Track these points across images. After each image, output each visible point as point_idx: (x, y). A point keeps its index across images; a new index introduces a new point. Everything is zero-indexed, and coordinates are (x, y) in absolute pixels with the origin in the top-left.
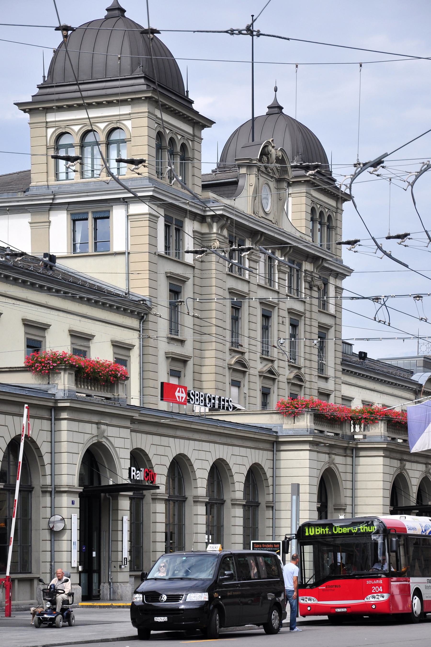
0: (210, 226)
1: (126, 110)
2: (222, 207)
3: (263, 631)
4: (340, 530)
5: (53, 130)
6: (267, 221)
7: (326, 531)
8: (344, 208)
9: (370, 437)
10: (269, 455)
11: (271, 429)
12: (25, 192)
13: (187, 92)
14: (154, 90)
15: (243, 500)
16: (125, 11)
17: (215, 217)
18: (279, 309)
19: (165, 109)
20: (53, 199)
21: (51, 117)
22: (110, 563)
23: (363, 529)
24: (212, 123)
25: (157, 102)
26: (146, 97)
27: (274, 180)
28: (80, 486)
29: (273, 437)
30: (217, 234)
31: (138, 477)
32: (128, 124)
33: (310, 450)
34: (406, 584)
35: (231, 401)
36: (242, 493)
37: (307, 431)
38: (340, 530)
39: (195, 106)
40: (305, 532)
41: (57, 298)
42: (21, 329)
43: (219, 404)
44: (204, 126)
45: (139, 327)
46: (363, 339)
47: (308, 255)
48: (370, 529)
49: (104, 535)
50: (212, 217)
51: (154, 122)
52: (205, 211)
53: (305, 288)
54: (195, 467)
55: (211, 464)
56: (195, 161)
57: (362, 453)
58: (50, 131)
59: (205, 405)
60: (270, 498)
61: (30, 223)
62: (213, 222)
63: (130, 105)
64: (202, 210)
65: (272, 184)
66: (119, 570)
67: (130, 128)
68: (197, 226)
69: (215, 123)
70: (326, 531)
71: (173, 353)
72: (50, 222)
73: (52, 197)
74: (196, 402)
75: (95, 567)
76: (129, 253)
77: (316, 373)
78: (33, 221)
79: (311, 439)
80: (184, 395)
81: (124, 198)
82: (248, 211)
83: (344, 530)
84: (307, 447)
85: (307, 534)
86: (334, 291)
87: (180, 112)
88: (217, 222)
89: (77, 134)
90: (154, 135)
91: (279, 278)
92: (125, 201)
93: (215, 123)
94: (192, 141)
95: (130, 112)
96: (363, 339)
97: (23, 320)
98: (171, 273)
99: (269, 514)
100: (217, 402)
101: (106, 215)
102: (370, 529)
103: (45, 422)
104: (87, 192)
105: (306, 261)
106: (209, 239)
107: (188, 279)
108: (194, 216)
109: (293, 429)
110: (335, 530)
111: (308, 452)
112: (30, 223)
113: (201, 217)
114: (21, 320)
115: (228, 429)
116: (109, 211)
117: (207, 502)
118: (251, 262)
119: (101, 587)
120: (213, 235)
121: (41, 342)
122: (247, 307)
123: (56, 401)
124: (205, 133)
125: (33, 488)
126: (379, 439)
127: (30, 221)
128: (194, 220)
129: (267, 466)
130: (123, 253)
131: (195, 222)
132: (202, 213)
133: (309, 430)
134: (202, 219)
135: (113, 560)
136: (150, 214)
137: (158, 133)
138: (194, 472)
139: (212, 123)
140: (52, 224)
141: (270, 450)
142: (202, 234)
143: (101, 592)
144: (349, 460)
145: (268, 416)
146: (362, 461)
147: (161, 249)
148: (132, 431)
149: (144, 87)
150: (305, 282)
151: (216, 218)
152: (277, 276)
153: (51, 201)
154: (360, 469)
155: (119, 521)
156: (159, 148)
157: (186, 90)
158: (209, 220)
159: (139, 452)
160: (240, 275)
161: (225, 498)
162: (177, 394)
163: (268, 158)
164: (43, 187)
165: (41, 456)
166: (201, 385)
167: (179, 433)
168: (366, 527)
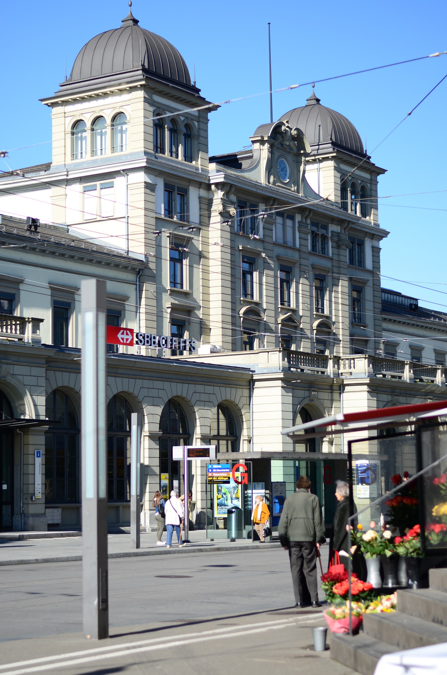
1: (126, 97)
3: (318, 558)
8: (209, 117)
9: (355, 374)
12: (45, 171)
13: (366, 151)
16: (320, 100)
17: (219, 185)
22: (22, 496)
26: (332, 157)
27: (292, 155)
37: (280, 369)
39: (372, 160)
47: (333, 218)
50: (217, 184)
53: (332, 247)
58: (68, 119)
66: (30, 502)
69: (387, 171)
72: (66, 195)
73: (66, 173)
76: (128, 217)
86: (198, 202)
89: (88, 120)
93: (387, 171)
104: (93, 167)
105: (332, 224)
107: (368, 281)
109: (267, 368)
113: (206, 185)
119: (14, 518)
122: (262, 263)
124: (380, 178)
130: (124, 217)
133: (281, 368)
135: (25, 492)
137: (362, 187)
143: (14, 523)
150: (332, 242)
157: (364, 149)
160: (323, 254)
164: (61, 166)
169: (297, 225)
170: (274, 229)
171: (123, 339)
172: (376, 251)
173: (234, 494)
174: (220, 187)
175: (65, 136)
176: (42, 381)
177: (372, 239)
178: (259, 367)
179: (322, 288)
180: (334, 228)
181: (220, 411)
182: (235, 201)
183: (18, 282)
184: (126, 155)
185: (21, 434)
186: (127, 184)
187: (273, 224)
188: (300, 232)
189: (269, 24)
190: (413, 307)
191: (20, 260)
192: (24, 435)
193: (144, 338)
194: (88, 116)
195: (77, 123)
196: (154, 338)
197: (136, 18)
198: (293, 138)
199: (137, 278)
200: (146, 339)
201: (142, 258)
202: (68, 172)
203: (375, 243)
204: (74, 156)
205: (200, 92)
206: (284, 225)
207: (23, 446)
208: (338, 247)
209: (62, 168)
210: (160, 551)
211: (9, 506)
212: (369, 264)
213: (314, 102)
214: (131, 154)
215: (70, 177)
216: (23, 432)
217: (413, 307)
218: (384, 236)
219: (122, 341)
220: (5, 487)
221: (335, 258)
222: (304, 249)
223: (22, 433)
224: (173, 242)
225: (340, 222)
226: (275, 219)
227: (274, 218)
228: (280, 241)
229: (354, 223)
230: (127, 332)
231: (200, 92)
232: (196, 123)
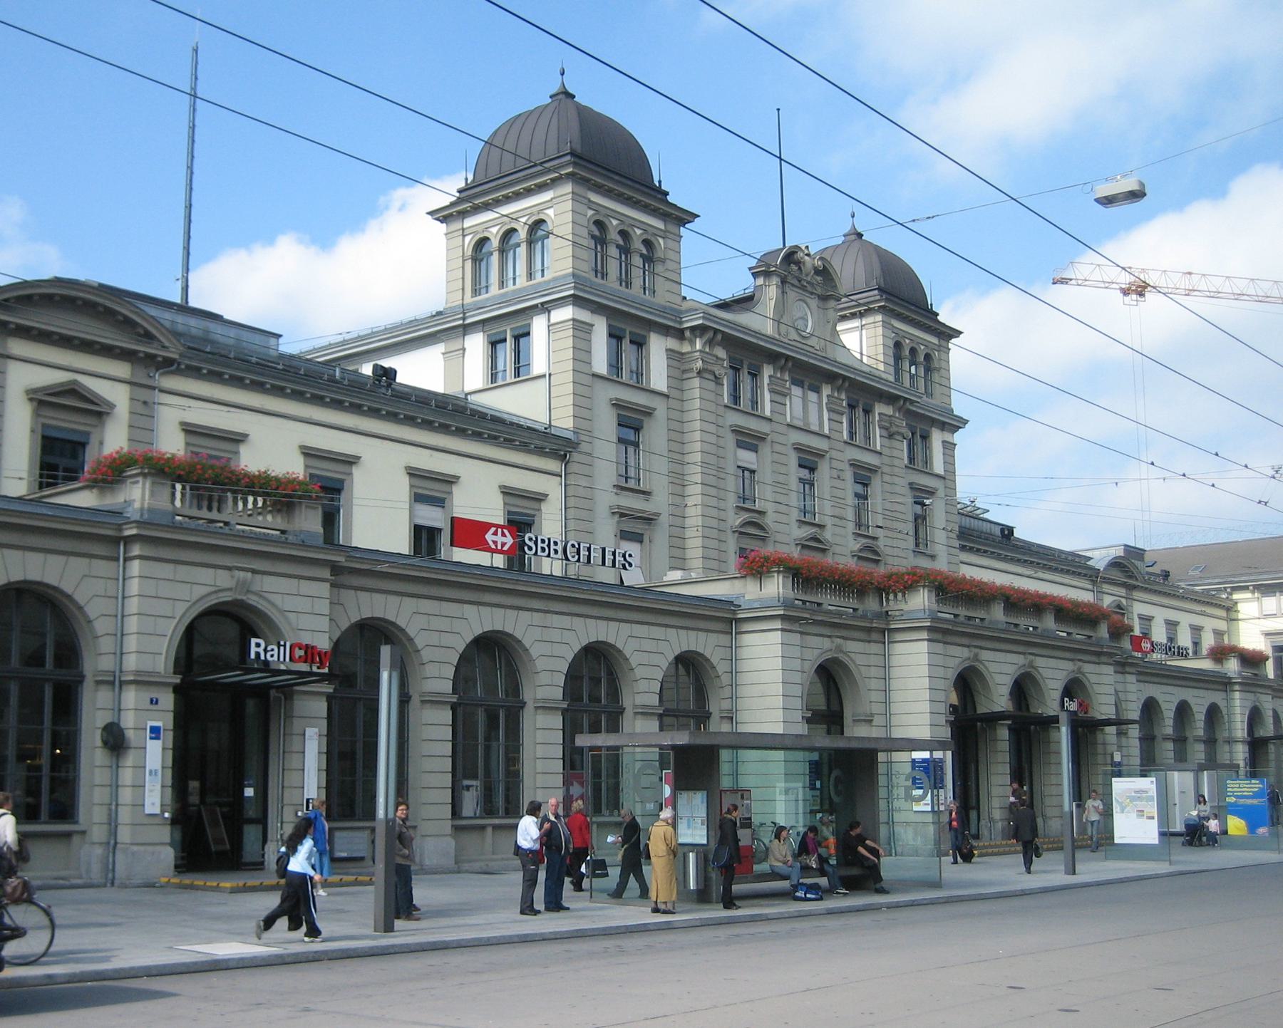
0: (692, 343)
1: (547, 196)
2: (701, 315)
5: (470, 237)
6: (804, 347)
10: (1223, 695)
11: (121, 513)
13: (931, 305)
14: (887, 300)
15: (453, 694)
18: (882, 473)
19: (598, 189)
20: (464, 319)
21: (469, 222)
24: (961, 333)
25: (892, 311)
26: (879, 307)
28: (175, 673)
29: (110, 529)
30: (700, 351)
31: (272, 656)
32: (550, 212)
33: (782, 630)
35: (630, 556)
36: (1172, 729)
41: (480, 443)
42: (405, 481)
43: (1179, 652)
44: (951, 337)
45: (559, 471)
49: (982, 768)
50: (693, 329)
51: (586, 207)
52: (681, 323)
53: (881, 436)
54: (1194, 710)
55: (1143, 701)
56: (943, 371)
57: (899, 637)
59: (1167, 654)
60: (726, 705)
61: (443, 354)
62: (696, 337)
63: (551, 189)
64: (675, 321)
65: (814, 303)
67: (553, 216)
68: (672, 343)
69: (699, 216)
71: (619, 507)
72: (464, 349)
73: (461, 316)
74: (539, 553)
75: (973, 802)
77: (851, 527)
78: (448, 350)
79: (782, 612)
80: (1149, 646)
81: (542, 304)
82: (769, 328)
84: (778, 625)
87: (931, 327)
88: (701, 337)
89: (495, 237)
90: (891, 344)
91: (842, 423)
92: (545, 308)
93: (699, 216)
94: (664, 238)
95: (552, 196)
97: (302, 447)
98: (617, 399)
99: (1226, 748)
100: (1176, 650)
101: (525, 331)
103: (721, 636)
106: (687, 360)
108: (666, 331)
109: (759, 600)
111: (780, 632)
112: (443, 354)
114: (404, 469)
115: (58, 519)
116: (529, 325)
117: (455, 703)
118: (831, 413)
120: (696, 354)
121: (342, 481)
122: (769, 454)
123: (1230, 678)
125: (1155, 736)
126: (921, 615)
127: (443, 351)
128: (667, 336)
129: (1222, 704)
130: (544, 376)
131: (669, 338)
132: (677, 326)
133: (781, 600)
134: (679, 334)
136: (574, 320)
138: (532, 660)
139: (961, 333)
140: (467, 350)
141: (726, 633)
142: (683, 354)
143: (266, 856)
144: (875, 648)
145: (727, 583)
146: (899, 648)
147: (601, 366)
148: (332, 585)
149: (878, 297)
150: (880, 428)
151: (699, 330)
152: (767, 396)
153: (461, 322)
154: (895, 661)
155: (294, 737)
156: (898, 358)
157: (929, 303)
158: (687, 334)
159: (505, 637)
161: (1156, 733)
162: (1143, 645)
163: (800, 268)
165: (1223, 717)
166: (684, 554)
167: (488, 598)
169: (825, 400)
170: (788, 403)
171: (495, 542)
172: (949, 447)
173: (401, 850)
174: (698, 333)
176: (324, 607)
177: (943, 430)
178: (746, 598)
181: (680, 666)
182: (725, 357)
183: (350, 461)
184: (549, 281)
187: (786, 396)
188: (830, 410)
189: (778, 110)
190: (1006, 532)
192: (286, 698)
193: (536, 543)
194: (494, 230)
195: (483, 242)
196: (556, 543)
197: (571, 91)
198: (817, 272)
200: (540, 545)
201: (570, 435)
202: (464, 314)
204: (476, 292)
206: (804, 399)
207: (285, 719)
210: (418, 944)
211: (260, 827)
212: (938, 467)
213: (853, 237)
214: (555, 279)
215: (468, 321)
217: (1006, 532)
218: (961, 426)
219: (493, 547)
220: (249, 792)
221: (886, 451)
222: (835, 435)
224: (927, 607)
225: (891, 399)
226: (790, 389)
227: (788, 386)
228: (799, 424)
229: (912, 402)
230: (503, 532)
232: (661, 241)
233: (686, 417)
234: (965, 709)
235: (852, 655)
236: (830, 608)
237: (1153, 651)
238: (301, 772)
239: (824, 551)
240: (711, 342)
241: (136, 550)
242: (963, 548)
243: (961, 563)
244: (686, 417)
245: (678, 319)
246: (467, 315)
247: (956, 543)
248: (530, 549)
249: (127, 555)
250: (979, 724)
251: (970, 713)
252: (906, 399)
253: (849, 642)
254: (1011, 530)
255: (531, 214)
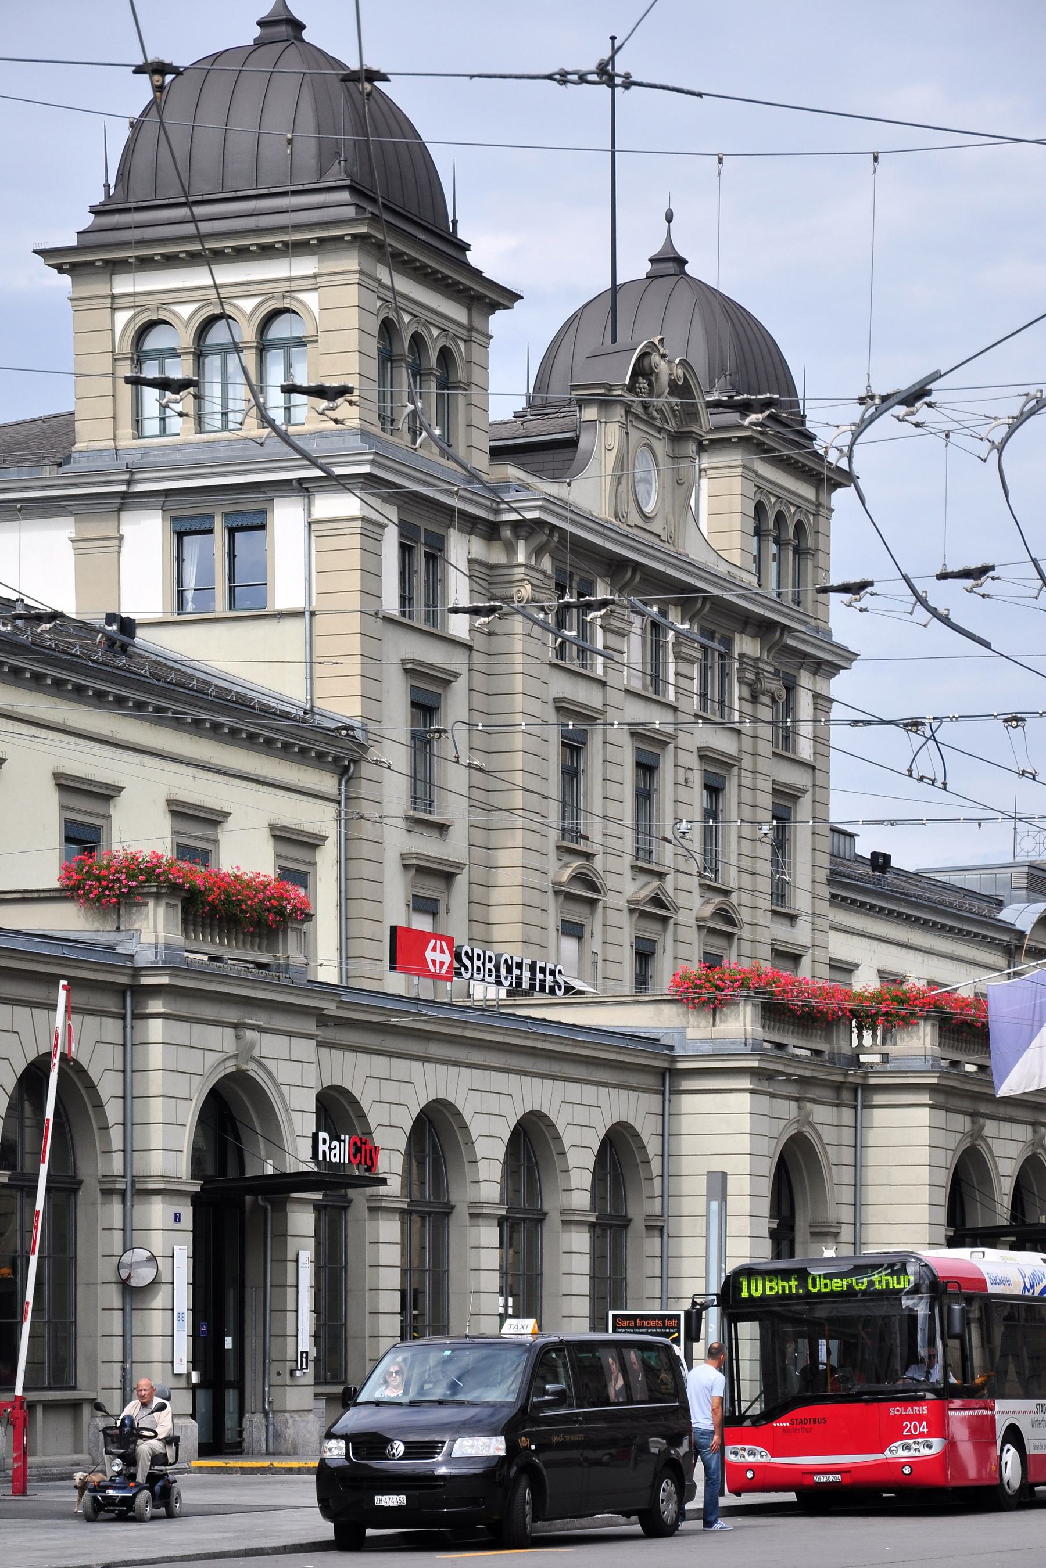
0: (510, 549)
1: (305, 266)
2: (540, 503)
4: (826, 1285)
5: (128, 314)
6: (647, 536)
7: (790, 1287)
9: (897, 1058)
10: (653, 1102)
11: (658, 1040)
12: (60, 465)
13: (455, 222)
17: (522, 526)
18: (676, 748)
19: (401, 263)
20: (129, 483)
21: (124, 285)
22: (267, 1365)
23: (880, 1282)
24: (516, 297)
25: (380, 246)
29: (662, 1060)
30: (526, 566)
32: (311, 300)
33: (752, 1091)
34: (986, 1416)
36: (587, 1196)
37: (746, 1045)
38: (826, 1285)
40: (741, 1290)
41: (137, 722)
42: (51, 798)
43: (532, 979)
44: (494, 307)
45: (336, 792)
46: (881, 822)
47: (748, 618)
48: (899, 1283)
50: (516, 525)
51: (374, 295)
52: (497, 512)
53: (740, 699)
54: (474, 1131)
55: (513, 1124)
56: (474, 390)
57: (879, 1099)
58: (122, 318)
59: (498, 983)
61: (73, 541)
62: (518, 538)
63: (315, 253)
65: (661, 447)
66: (288, 1382)
67: (316, 311)
68: (477, 548)
69: (522, 298)
70: (790, 1287)
72: (121, 538)
73: (126, 477)
76: (312, 614)
78: (80, 537)
79: (755, 1064)
80: (447, 958)
81: (300, 481)
82: (603, 511)
83: (834, 1285)
84: (745, 1083)
85: (745, 1294)
87: (436, 271)
88: (526, 539)
89: (187, 325)
90: (374, 326)
91: (677, 674)
93: (522, 298)
94: (465, 341)
95: (316, 271)
96: (881, 822)
97: (57, 776)
98: (414, 661)
99: (653, 1245)
101: (257, 522)
102: (899, 1283)
104: (211, 466)
105: (742, 632)
106: (508, 578)
108: (472, 524)
110: (814, 1285)
111: (748, 1094)
112: (73, 541)
113: (487, 526)
114: (50, 777)
115: (553, 1040)
116: (264, 512)
118: (609, 635)
119: (246, 1423)
120: (517, 570)
121: (99, 828)
122: (601, 745)
123: (137, 972)
126: (919, 1065)
127: (73, 535)
128: (470, 534)
129: (647, 1129)
130: (300, 614)
131: (473, 537)
132: (491, 517)
133: (750, 1041)
134: (491, 531)
136: (364, 519)
139: (516, 297)
141: (656, 1092)
142: (491, 567)
143: (245, 1435)
145: (650, 1009)
146: (879, 1116)
148: (319, 1044)
149: (350, 212)
150: (740, 683)
152: (671, 668)
153: (123, 488)
156: (387, 358)
157: (451, 218)
158: (507, 533)
162: (429, 955)
164: (105, 453)
166: (489, 933)
167: (435, 1049)
168: (889, 1278)
175: (114, 367)
179: (716, 811)
180: (746, 645)
185: (265, 1209)
186: (310, 520)
188: (678, 656)
191: (110, 734)
199: (340, 785)
203: (821, 685)
205: (467, 253)
208: (754, 699)
209: (107, 458)
212: (805, 750)
216: (271, 1203)
223: (269, 1207)
231: (467, 253)
233: (499, 684)
234: (222, 1169)
235: (270, 1064)
236: (798, 1051)
237: (459, 974)
238: (295, 1338)
239: (665, 920)
240: (538, 552)
241: (156, 1006)
242: (834, 900)
243: (831, 928)
244: (499, 684)
245: (494, 505)
246: (137, 476)
247: (825, 891)
248: (466, 968)
249: (136, 1012)
250: (249, 1199)
251: (232, 1173)
252: (785, 628)
253: (266, 1038)
254: (887, 858)
255: (270, 296)
